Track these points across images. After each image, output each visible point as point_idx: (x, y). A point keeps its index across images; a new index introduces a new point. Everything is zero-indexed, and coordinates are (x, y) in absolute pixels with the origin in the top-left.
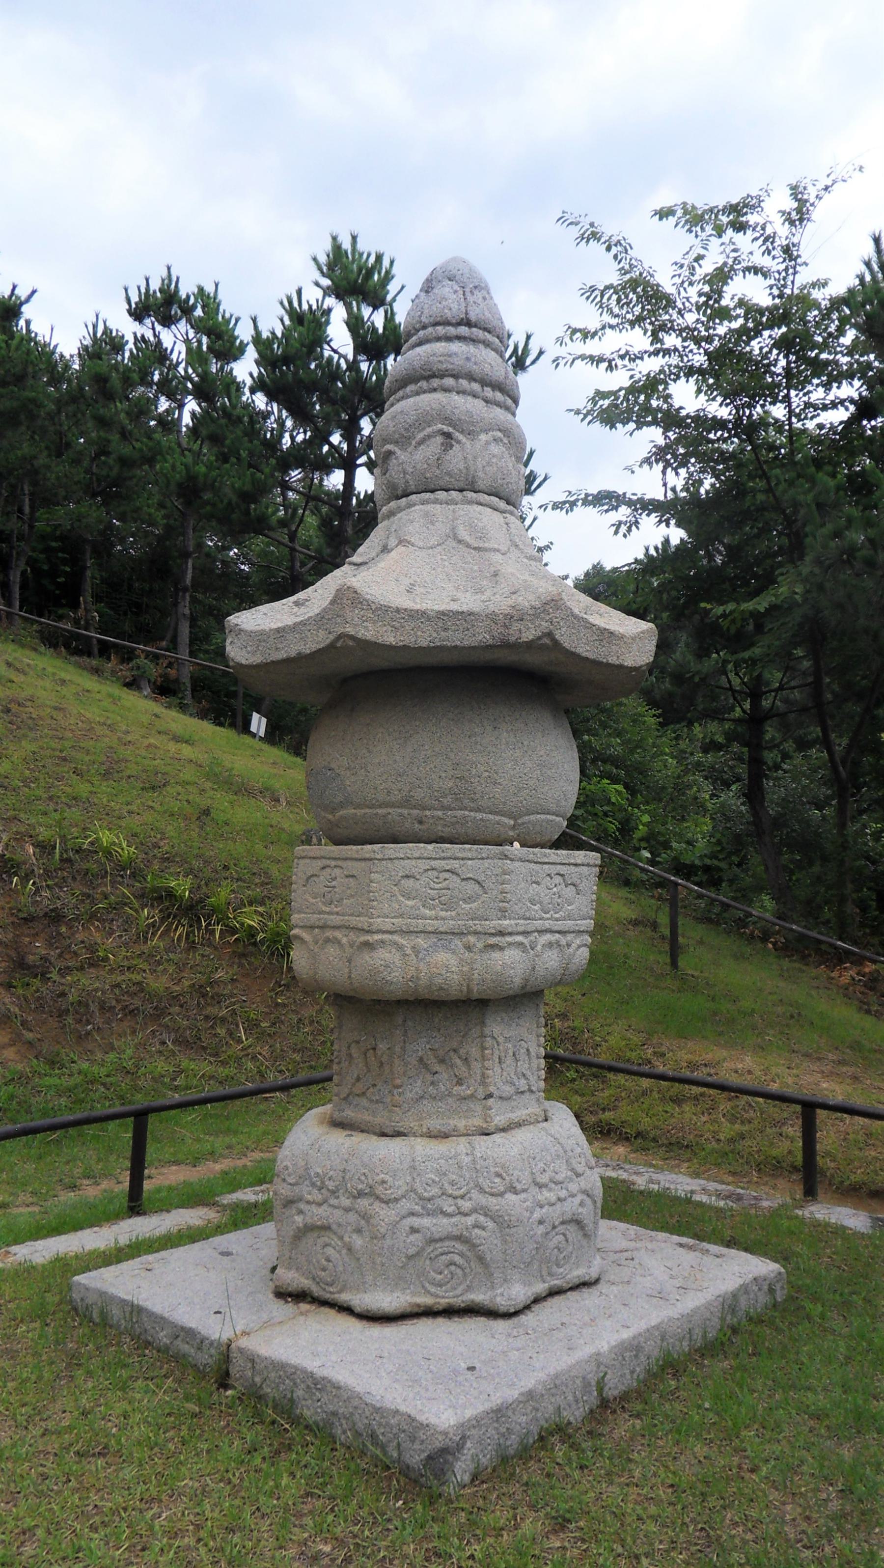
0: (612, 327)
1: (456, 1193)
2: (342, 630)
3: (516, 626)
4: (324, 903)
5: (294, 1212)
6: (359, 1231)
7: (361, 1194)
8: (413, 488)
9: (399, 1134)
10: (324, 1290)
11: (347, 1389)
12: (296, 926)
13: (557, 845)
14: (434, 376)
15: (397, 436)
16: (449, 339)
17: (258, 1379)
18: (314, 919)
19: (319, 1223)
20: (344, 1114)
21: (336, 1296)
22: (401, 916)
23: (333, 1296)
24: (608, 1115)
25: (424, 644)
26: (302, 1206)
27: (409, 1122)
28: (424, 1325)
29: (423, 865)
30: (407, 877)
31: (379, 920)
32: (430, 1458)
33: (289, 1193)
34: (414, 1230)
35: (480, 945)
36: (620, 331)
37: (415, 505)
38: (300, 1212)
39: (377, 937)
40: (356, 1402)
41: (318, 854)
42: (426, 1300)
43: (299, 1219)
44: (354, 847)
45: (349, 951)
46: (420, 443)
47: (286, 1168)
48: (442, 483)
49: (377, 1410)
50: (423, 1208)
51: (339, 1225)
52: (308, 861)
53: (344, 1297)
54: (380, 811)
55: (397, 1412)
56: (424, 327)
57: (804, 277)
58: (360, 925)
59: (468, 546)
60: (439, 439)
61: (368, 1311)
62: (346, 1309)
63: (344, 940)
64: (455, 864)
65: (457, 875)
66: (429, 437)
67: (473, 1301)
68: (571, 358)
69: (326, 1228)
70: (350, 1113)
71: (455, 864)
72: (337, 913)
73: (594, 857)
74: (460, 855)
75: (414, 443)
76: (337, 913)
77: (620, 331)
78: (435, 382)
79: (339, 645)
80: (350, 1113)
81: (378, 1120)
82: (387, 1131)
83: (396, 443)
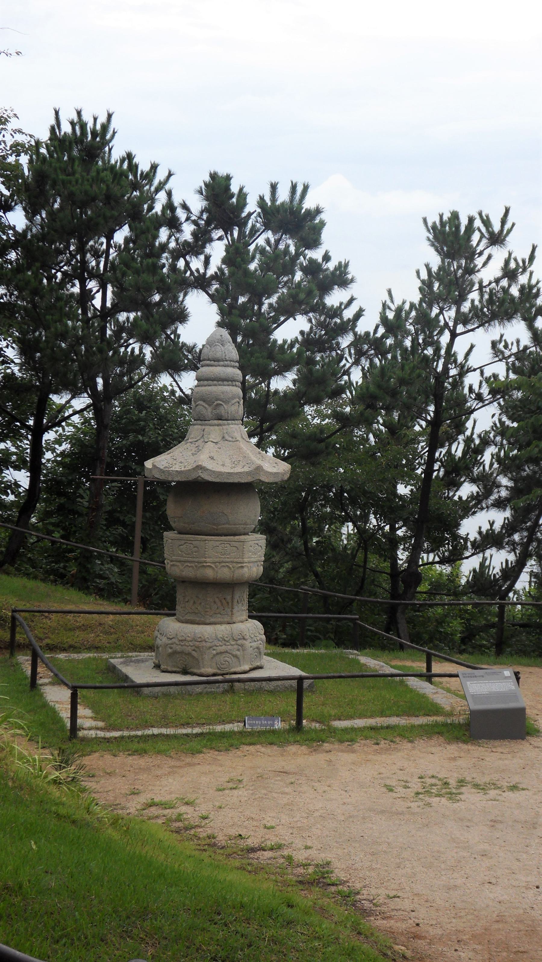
6: (238, 650)
7: (240, 639)
26: (215, 648)
27: (234, 619)
42: (251, 666)
43: (214, 652)
53: (233, 670)
69: (227, 652)
81: (226, 620)
83: (223, 402)
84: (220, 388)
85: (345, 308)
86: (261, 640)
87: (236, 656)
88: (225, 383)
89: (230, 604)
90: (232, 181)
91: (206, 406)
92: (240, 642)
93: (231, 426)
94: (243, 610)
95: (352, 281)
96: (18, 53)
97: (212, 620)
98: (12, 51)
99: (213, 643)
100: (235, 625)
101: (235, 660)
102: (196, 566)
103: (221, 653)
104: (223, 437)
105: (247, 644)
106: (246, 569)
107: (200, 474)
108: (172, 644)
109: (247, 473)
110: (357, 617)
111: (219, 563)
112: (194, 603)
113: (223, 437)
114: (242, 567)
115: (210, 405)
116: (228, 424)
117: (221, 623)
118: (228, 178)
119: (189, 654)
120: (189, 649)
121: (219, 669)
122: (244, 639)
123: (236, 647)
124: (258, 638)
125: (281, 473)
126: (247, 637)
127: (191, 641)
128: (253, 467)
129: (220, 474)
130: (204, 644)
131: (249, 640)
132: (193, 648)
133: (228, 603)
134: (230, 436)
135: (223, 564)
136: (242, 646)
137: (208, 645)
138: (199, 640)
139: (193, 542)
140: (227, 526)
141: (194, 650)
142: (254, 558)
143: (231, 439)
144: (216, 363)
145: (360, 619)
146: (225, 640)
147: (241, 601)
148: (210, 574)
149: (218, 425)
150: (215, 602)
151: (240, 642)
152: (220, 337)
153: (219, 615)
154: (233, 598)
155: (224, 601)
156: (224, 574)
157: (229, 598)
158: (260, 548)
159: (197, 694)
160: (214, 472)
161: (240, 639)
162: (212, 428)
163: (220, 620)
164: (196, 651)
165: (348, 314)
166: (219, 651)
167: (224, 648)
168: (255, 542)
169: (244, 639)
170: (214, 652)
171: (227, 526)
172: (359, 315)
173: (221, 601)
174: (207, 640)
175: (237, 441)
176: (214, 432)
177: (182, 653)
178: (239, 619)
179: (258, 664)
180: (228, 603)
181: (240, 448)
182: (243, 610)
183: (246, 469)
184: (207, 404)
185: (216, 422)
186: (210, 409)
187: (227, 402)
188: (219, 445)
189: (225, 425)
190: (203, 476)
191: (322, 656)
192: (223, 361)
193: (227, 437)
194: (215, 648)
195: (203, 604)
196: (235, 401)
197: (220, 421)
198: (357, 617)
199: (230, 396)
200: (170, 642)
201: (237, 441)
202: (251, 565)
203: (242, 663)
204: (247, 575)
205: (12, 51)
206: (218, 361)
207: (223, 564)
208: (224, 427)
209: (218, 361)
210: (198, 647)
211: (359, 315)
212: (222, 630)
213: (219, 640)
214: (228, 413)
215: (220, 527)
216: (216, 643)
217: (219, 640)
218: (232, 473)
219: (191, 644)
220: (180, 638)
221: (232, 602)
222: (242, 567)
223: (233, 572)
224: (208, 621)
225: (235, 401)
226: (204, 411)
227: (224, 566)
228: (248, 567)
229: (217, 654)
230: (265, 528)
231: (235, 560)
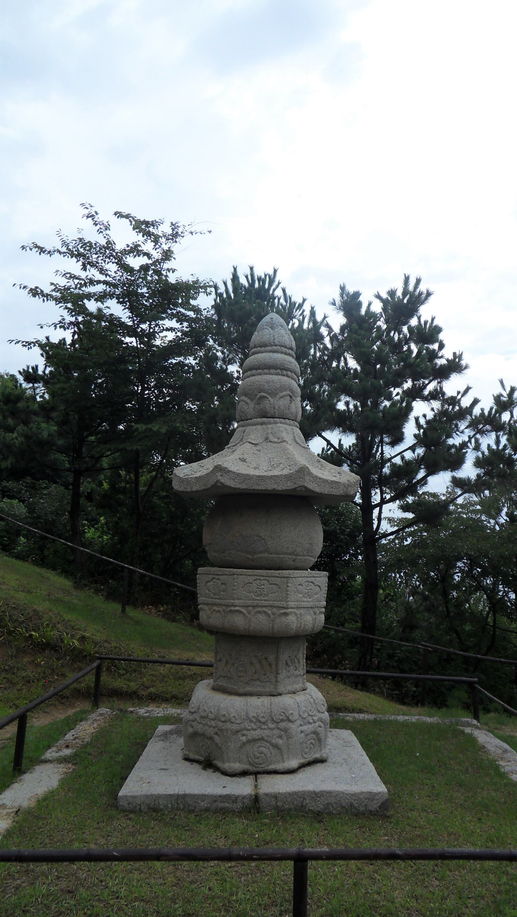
0: (60, 252)
1: (312, 714)
2: (303, 484)
3: (350, 489)
4: (255, 595)
5: (240, 736)
6: (280, 737)
7: (282, 721)
8: (277, 416)
9: (280, 695)
10: (258, 767)
11: (335, 792)
12: (201, 604)
13: (312, 569)
14: (284, 369)
15: (270, 391)
16: (286, 354)
17: (279, 804)
18: (210, 600)
19: (257, 738)
20: (246, 689)
21: (267, 768)
22: (297, 601)
23: (263, 769)
24: (152, 689)
25: (326, 493)
26: (245, 732)
27: (281, 689)
28: (309, 770)
29: (305, 580)
30: (299, 585)
31: (291, 603)
32: (382, 804)
33: (237, 728)
34: (302, 732)
35: (318, 612)
36: (64, 256)
37: (278, 423)
38: (244, 735)
39: (290, 610)
40: (342, 795)
41: (253, 574)
42: (303, 761)
43: (244, 739)
44: (245, 570)
45: (272, 617)
46: (281, 397)
47: (234, 717)
48: (288, 416)
49: (353, 795)
50: (304, 722)
51: (268, 736)
52: (245, 576)
53: (272, 767)
54: (282, 556)
55: (363, 792)
56: (276, 346)
57: (167, 265)
58: (281, 605)
59: (301, 446)
60: (288, 398)
61: (288, 769)
62: (276, 772)
63: (270, 612)
64: (312, 579)
65: (314, 583)
66: (285, 396)
67: (315, 758)
68: (64, 273)
69: (262, 739)
70: (249, 689)
71: (312, 579)
72: (265, 600)
73: (327, 573)
74: (316, 576)
75: (278, 396)
76: (265, 600)
77: (64, 256)
78: (285, 372)
79: (298, 489)
80: (249, 689)
81: (267, 690)
82: (275, 693)
83: (269, 394)
84: (265, 377)
85: (462, 396)
86: (321, 720)
87: (276, 746)
88: (272, 371)
89: (274, 667)
90: (361, 298)
91: (248, 401)
92: (282, 725)
93: (279, 425)
94: (297, 676)
95: (466, 367)
96: (210, 232)
97: (249, 689)
98: (205, 231)
99: (242, 726)
100: (279, 698)
101: (274, 751)
102: (224, 611)
103: (255, 740)
104: (267, 439)
105: (294, 727)
106: (292, 618)
107: (220, 478)
108: (193, 721)
109: (285, 476)
110: (476, 679)
111: (253, 606)
112: (227, 662)
113: (267, 439)
114: (286, 614)
115: (252, 400)
116: (275, 423)
117: (259, 695)
118: (357, 295)
119: (211, 738)
120: (210, 732)
121: (250, 764)
122: (290, 721)
123: (276, 732)
124: (316, 718)
125: (344, 485)
126: (296, 717)
127: (213, 720)
128: (296, 468)
129: (247, 477)
130: (229, 725)
131: (299, 722)
132: (216, 730)
133: (270, 665)
134: (275, 437)
135: (260, 609)
136: (286, 730)
137: (235, 727)
138: (223, 719)
139: (221, 577)
140: (266, 555)
141: (216, 734)
142: (307, 602)
143: (276, 440)
144: (263, 349)
145: (479, 683)
146: (260, 722)
147: (293, 662)
148: (239, 622)
149: (262, 424)
150: (252, 663)
151: (282, 725)
152: (270, 320)
153: (258, 683)
154: (277, 659)
155: (264, 662)
156: (260, 623)
157: (272, 658)
158: (318, 589)
159: (201, 810)
160: (238, 475)
161: (282, 721)
162: (253, 427)
163: (259, 689)
164: (219, 736)
165: (466, 402)
166: (250, 738)
167: (257, 734)
168: (308, 579)
169: (290, 721)
170: (244, 739)
171: (266, 555)
172: (476, 402)
173: (260, 662)
174: (233, 720)
175: (284, 441)
176: (255, 433)
177: (203, 735)
178: (289, 688)
179: (317, 756)
180: (270, 665)
181: (285, 450)
182: (297, 676)
183: (286, 472)
184: (249, 398)
185: (259, 420)
186: (252, 405)
187: (273, 393)
188: (258, 448)
189: (270, 423)
190: (223, 481)
191: (427, 729)
192: (272, 346)
193: (271, 438)
194: (245, 732)
195: (236, 665)
196: (284, 393)
197: (265, 419)
198: (476, 679)
199: (278, 386)
200: (191, 717)
201: (284, 441)
202: (302, 611)
203: (285, 756)
204: (294, 626)
205: (205, 231)
206: (265, 345)
207: (260, 609)
208: (270, 426)
209: (265, 345)
210: (221, 730)
211: (476, 402)
212: (258, 704)
213: (251, 721)
214: (274, 408)
215: (256, 556)
216: (247, 725)
217: (251, 721)
218: (264, 476)
219: (213, 723)
220: (203, 714)
221: (277, 665)
222: (286, 614)
223: (273, 621)
224: (241, 691)
225: (284, 393)
226: (246, 407)
227: (259, 612)
228: (296, 614)
229: (249, 741)
230: (326, 562)
231: (276, 604)
